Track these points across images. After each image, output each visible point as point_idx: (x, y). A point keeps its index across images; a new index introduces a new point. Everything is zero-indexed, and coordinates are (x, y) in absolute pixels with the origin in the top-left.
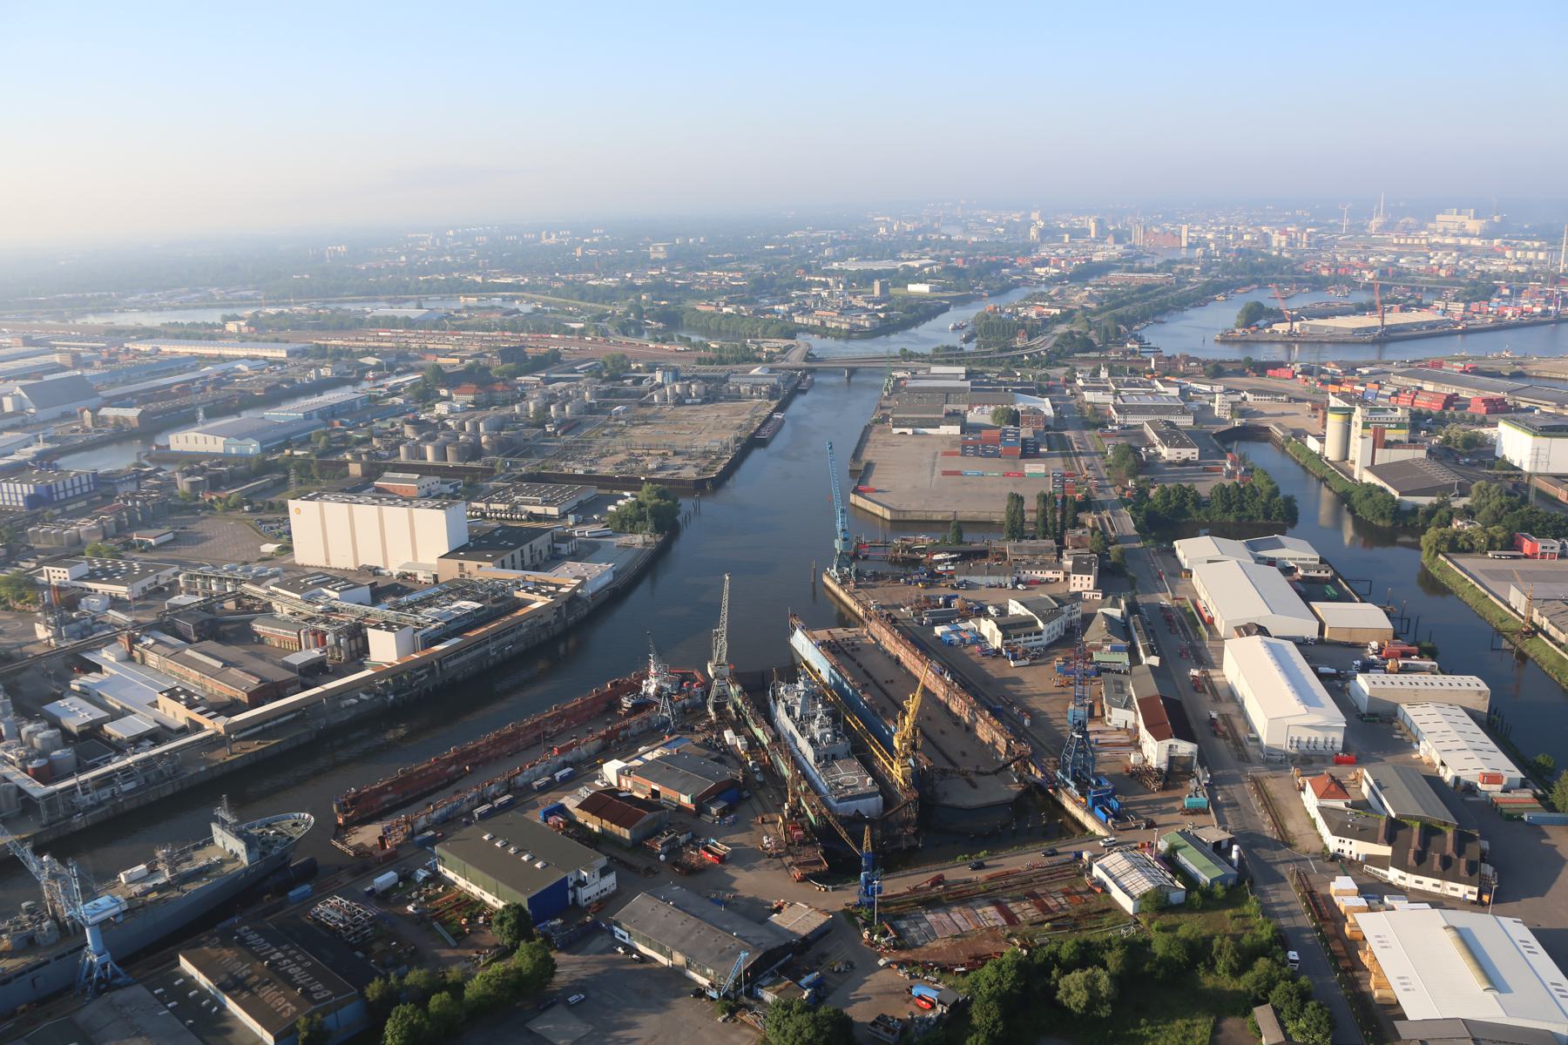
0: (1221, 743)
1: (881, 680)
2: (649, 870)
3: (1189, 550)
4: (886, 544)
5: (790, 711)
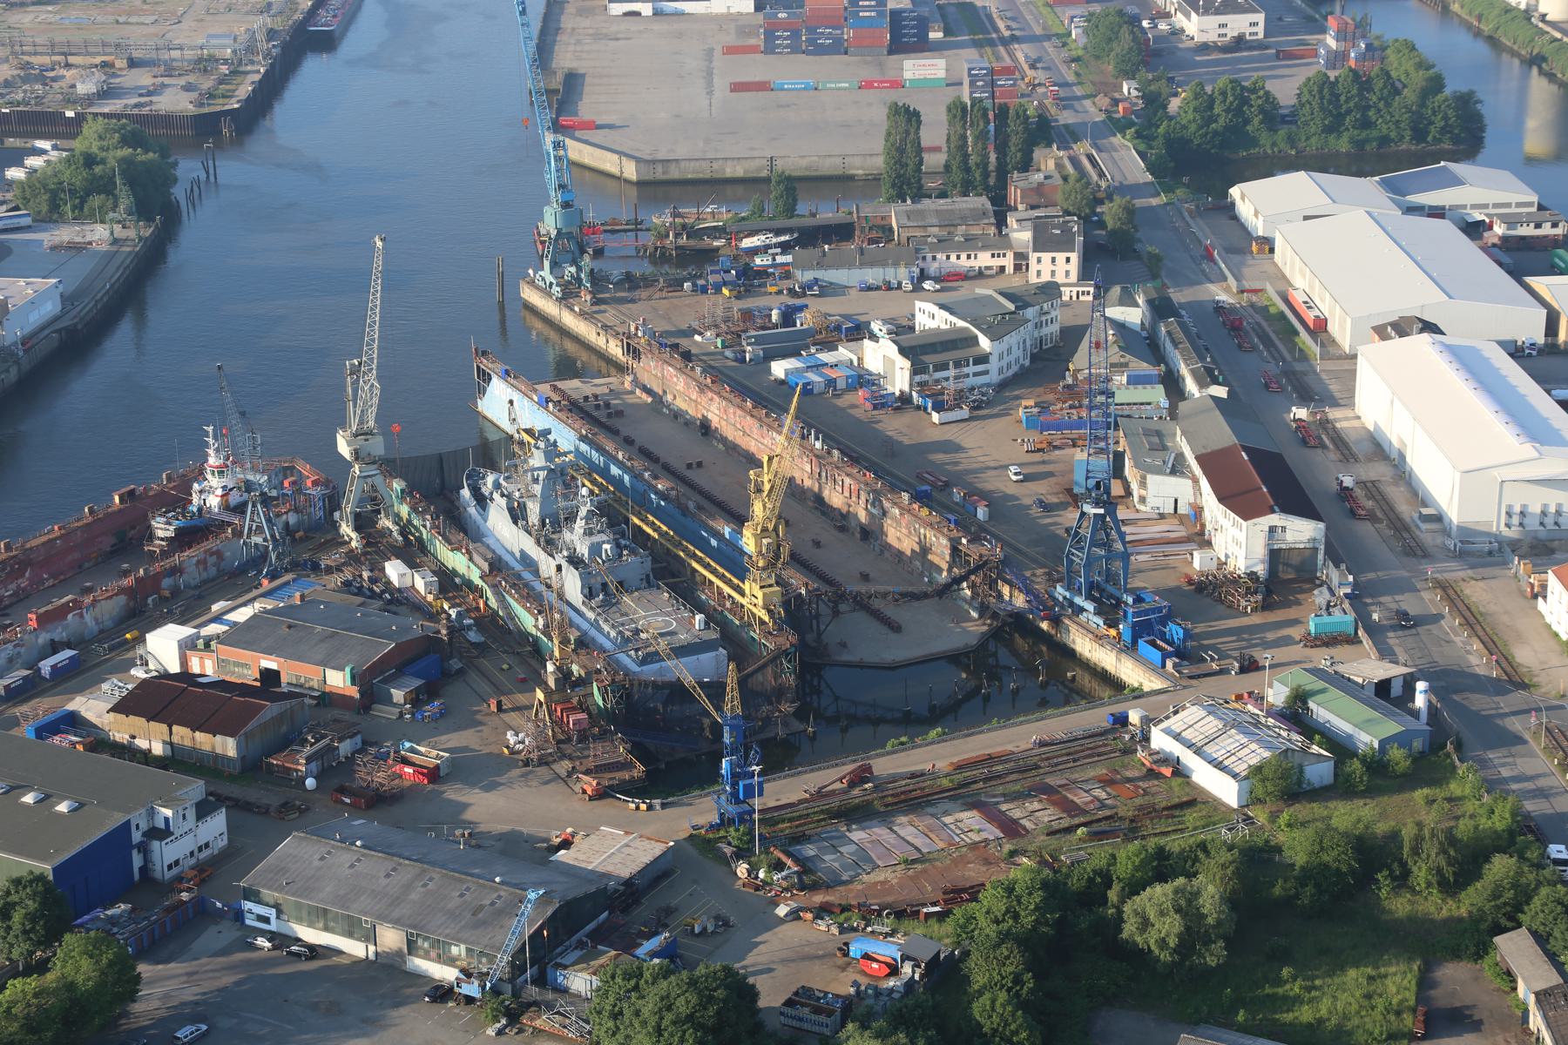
0: (1365, 529)
1: (678, 465)
2: (286, 807)
3: (1254, 201)
4: (637, 226)
5: (517, 514)
